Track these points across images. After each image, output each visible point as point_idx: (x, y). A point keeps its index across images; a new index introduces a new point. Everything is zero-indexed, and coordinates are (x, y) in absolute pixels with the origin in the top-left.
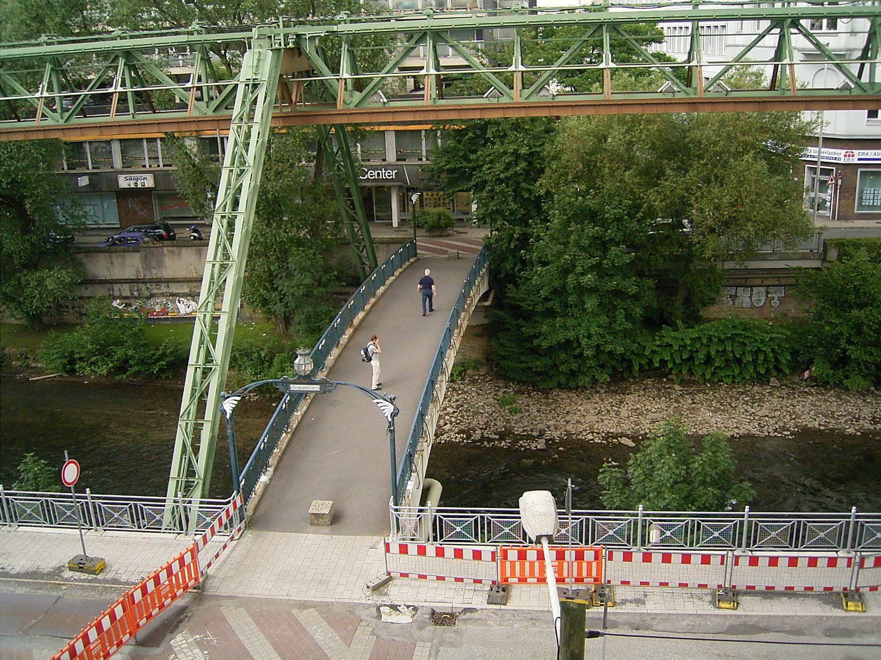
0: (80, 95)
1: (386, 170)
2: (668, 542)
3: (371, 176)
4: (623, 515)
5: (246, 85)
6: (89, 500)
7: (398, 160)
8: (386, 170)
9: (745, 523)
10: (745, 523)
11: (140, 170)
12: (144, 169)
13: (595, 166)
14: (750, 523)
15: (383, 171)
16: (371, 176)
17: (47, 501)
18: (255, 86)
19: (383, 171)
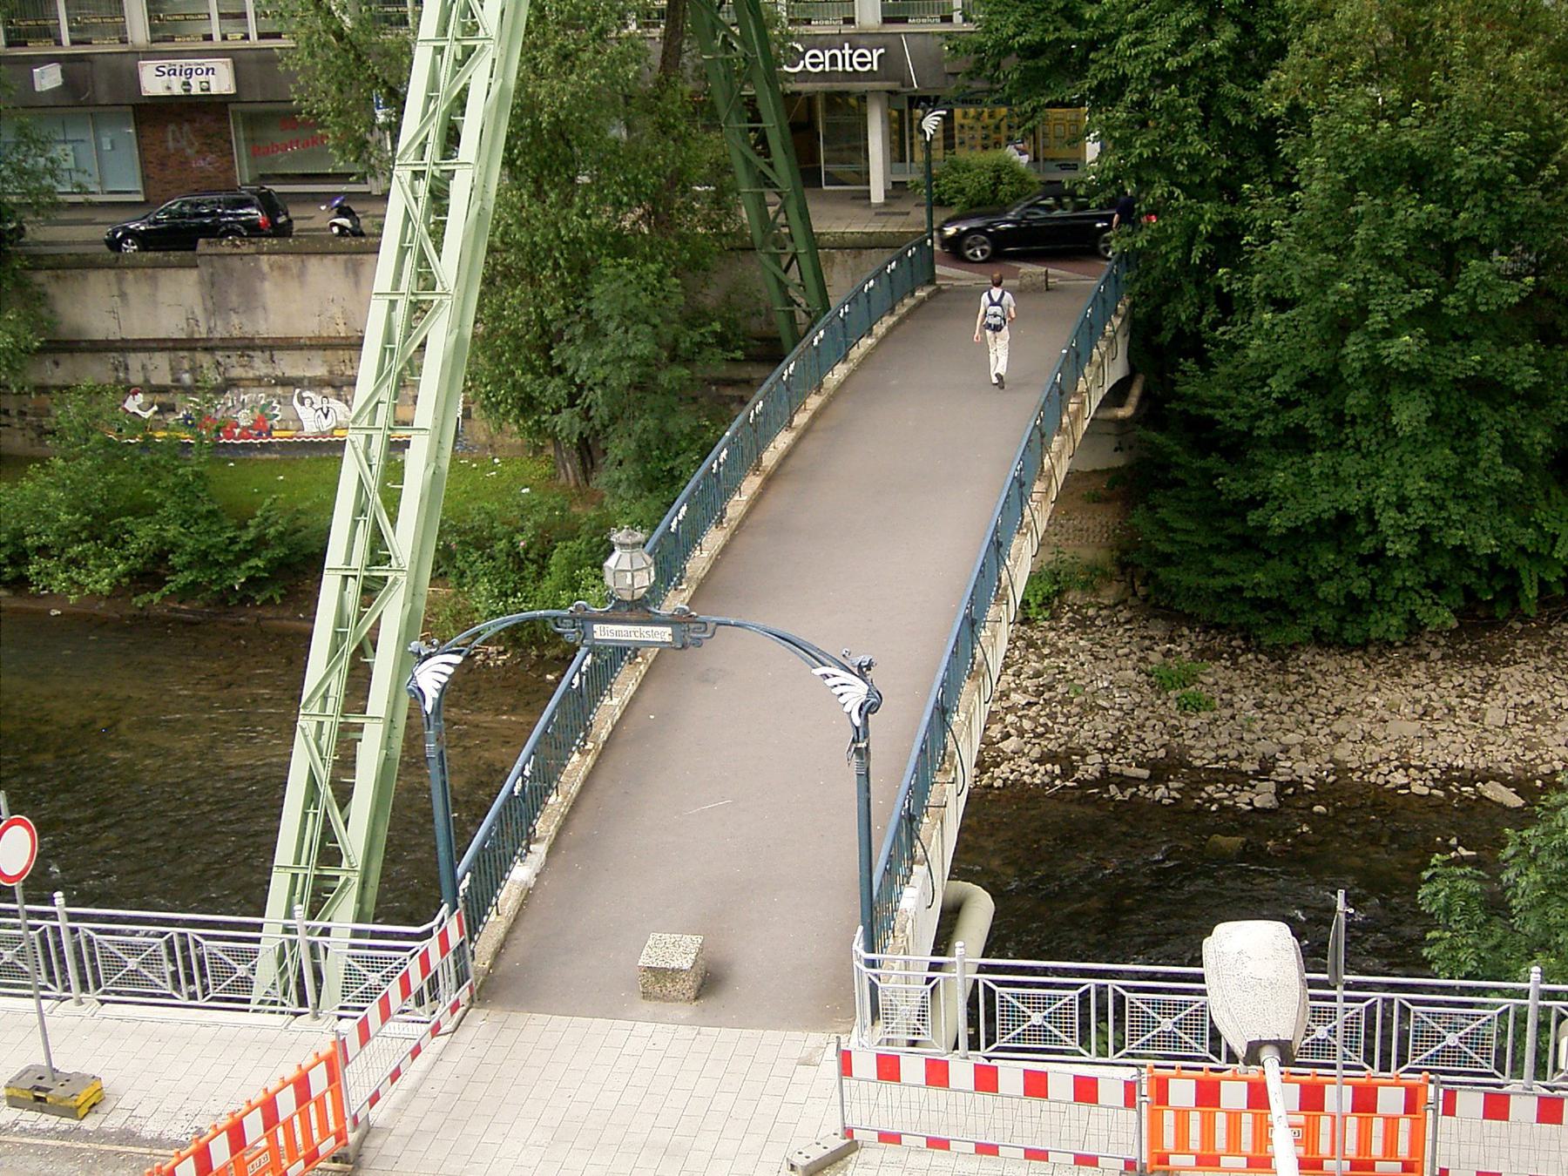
7: (886, 20)
15: (847, 51)
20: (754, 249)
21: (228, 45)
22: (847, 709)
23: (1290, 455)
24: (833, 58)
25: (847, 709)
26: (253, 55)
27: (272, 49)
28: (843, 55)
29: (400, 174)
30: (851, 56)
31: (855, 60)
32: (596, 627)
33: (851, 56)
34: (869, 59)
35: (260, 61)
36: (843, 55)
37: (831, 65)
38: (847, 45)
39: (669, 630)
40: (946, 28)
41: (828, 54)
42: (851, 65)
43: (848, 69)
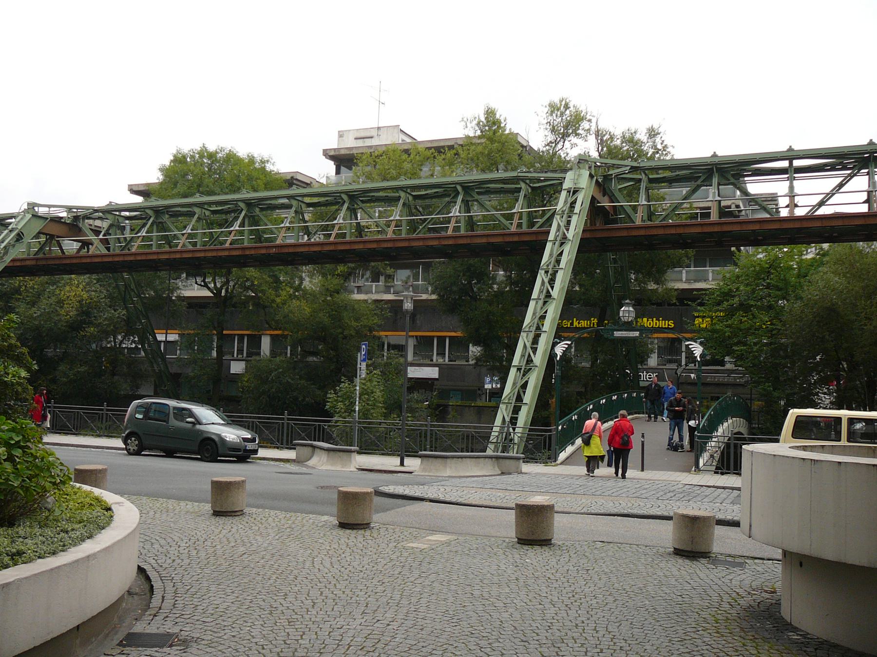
0: (428, 218)
1: (647, 373)
2: (304, 428)
3: (650, 378)
4: (242, 417)
5: (568, 192)
6: (286, 422)
7: (658, 364)
8: (647, 373)
9: (285, 425)
10: (285, 425)
11: (428, 363)
12: (431, 363)
13: (366, 390)
14: (288, 424)
15: (645, 374)
16: (650, 378)
17: (288, 424)
18: (575, 192)
19: (645, 374)
31: (647, 377)
42: (646, 378)
43: (645, 379)
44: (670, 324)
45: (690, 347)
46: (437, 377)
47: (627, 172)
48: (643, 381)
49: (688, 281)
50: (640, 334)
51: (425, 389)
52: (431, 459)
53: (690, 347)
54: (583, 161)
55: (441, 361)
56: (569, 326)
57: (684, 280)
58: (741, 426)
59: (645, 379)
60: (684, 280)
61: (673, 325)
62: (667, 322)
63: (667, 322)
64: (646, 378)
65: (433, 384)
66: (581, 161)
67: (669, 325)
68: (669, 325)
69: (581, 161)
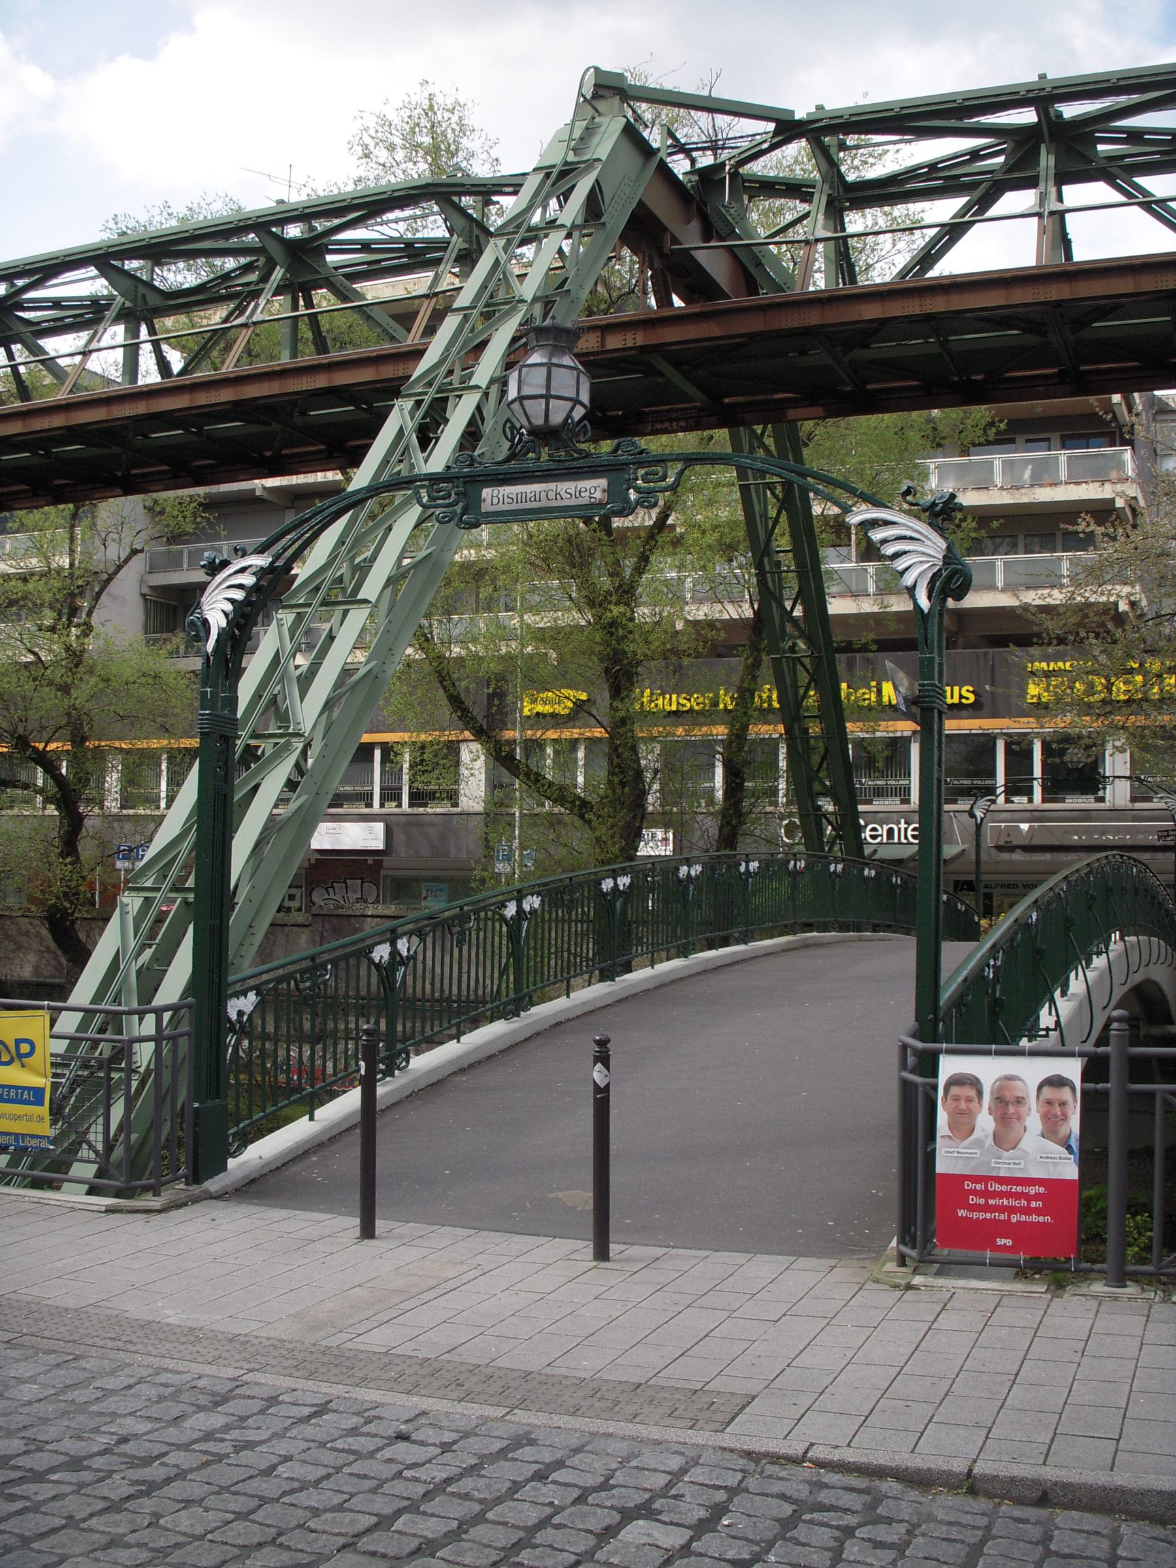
15: (903, 826)
20: (1112, 1470)
21: (384, 811)
22: (909, 580)
23: (267, 622)
24: (890, 832)
25: (909, 580)
26: (403, 819)
27: (272, 817)
28: (899, 829)
29: (125, 900)
30: (906, 829)
31: (910, 833)
32: (486, 492)
33: (906, 829)
34: (880, 833)
35: (408, 824)
36: (899, 829)
37: (888, 838)
38: (903, 821)
39: (602, 483)
40: (905, 807)
41: (886, 828)
42: (906, 838)
43: (903, 840)
44: (964, 693)
45: (877, 535)
46: (381, 848)
47: (765, 146)
48: (900, 843)
49: (1009, 588)
50: (608, 491)
51: (362, 879)
52: (509, 1044)
53: (877, 535)
54: (608, 93)
55: (390, 808)
56: (885, 840)
57: (1000, 584)
58: (1154, 959)
59: (903, 840)
60: (1000, 584)
61: (972, 698)
62: (956, 689)
63: (956, 689)
64: (906, 838)
65: (379, 865)
66: (601, 92)
67: (961, 697)
68: (961, 697)
69: (601, 92)
